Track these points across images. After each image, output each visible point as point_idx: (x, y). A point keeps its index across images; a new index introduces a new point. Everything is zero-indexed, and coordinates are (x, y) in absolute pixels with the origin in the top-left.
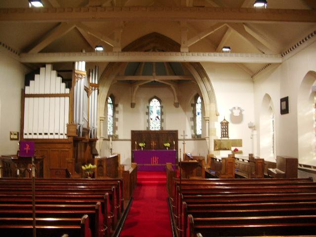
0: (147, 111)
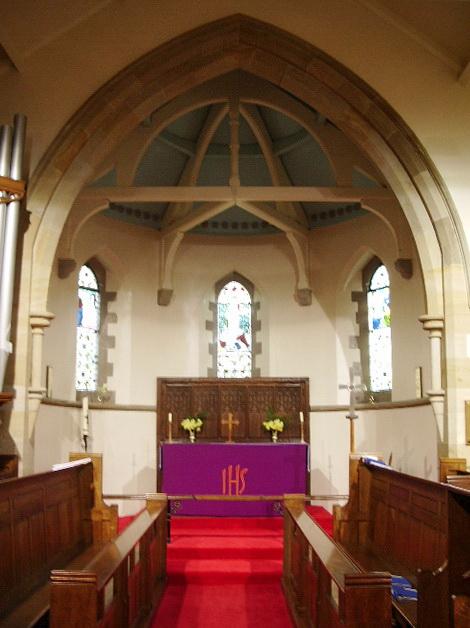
0: (211, 319)
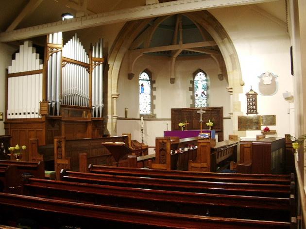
0: (191, 87)
